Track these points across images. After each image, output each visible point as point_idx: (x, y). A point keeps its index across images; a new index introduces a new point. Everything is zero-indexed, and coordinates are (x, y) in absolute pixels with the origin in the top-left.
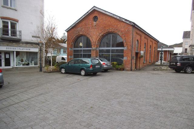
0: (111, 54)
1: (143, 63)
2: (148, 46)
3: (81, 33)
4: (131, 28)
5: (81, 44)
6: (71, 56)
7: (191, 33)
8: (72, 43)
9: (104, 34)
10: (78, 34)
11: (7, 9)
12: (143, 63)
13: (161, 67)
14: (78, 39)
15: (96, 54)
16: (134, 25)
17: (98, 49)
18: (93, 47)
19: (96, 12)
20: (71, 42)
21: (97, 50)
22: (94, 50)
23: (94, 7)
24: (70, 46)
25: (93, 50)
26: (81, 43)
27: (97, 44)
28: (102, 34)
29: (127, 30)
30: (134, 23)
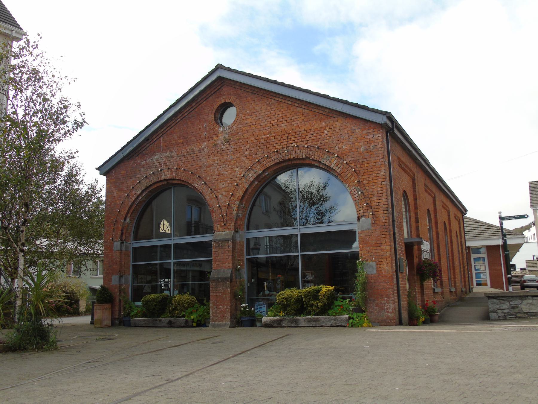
0: (300, 254)
1: (434, 292)
2: (152, 342)
3: (165, 176)
4: (379, 136)
5: (165, 226)
6: (121, 276)
7: (486, 286)
8: (128, 220)
9: (264, 171)
10: (153, 179)
11: (374, 113)
12: (434, 292)
13: (516, 302)
14: (154, 203)
15: (233, 257)
16: (390, 124)
17: (243, 236)
18: (217, 227)
19: (225, 89)
20: (124, 213)
21: (238, 240)
22: (222, 241)
23: (219, 67)
24: (119, 233)
25: (222, 242)
26: (165, 222)
27: (237, 216)
28: (259, 170)
29: (362, 149)
30: (389, 117)
